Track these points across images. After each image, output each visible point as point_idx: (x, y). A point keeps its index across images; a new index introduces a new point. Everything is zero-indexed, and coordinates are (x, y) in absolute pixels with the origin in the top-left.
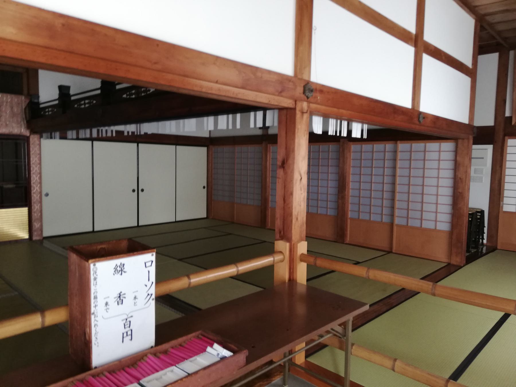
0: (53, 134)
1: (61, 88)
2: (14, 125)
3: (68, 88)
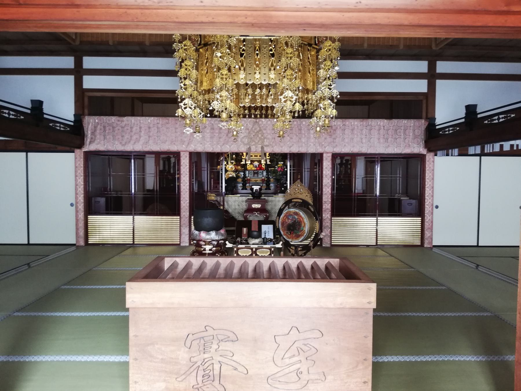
0: (450, 151)
1: (468, 107)
2: (415, 145)
3: (475, 106)
